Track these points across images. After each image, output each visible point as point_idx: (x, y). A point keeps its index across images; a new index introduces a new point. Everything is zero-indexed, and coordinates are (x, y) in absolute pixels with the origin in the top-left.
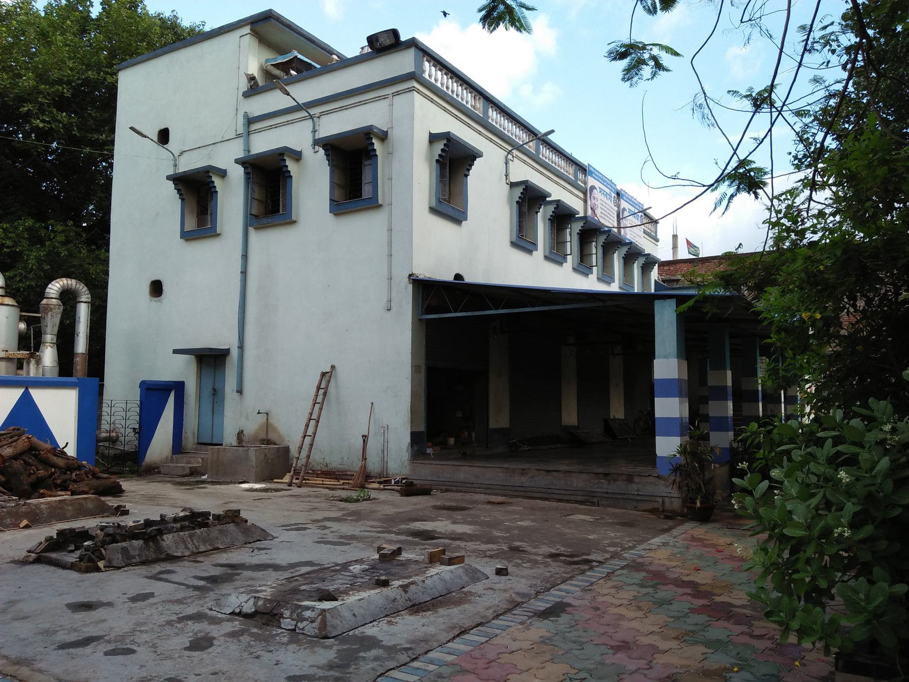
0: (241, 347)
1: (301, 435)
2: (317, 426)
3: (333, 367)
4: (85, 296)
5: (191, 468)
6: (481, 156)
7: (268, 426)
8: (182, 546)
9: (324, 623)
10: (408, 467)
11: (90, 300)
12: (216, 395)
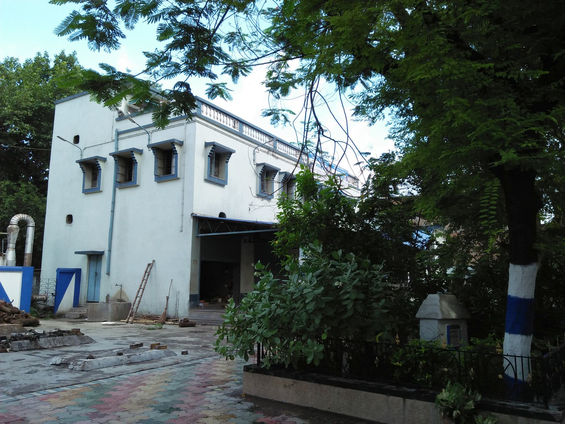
0: (110, 251)
1: (135, 296)
2: (143, 292)
3: (154, 261)
4: (32, 223)
5: (80, 314)
6: (234, 152)
7: (121, 292)
8: (48, 343)
9: (84, 366)
10: (188, 313)
11: (34, 225)
12: (97, 275)
